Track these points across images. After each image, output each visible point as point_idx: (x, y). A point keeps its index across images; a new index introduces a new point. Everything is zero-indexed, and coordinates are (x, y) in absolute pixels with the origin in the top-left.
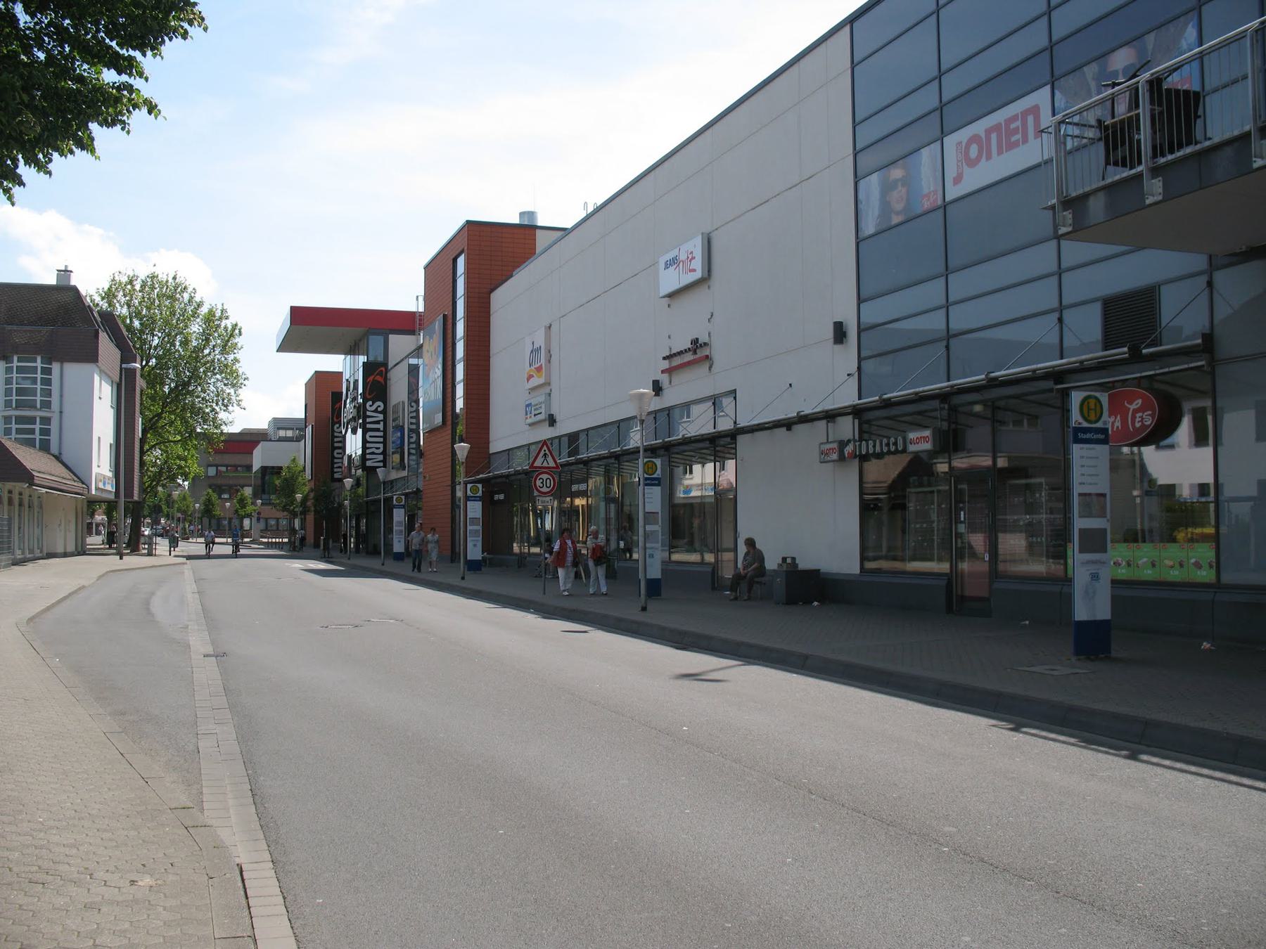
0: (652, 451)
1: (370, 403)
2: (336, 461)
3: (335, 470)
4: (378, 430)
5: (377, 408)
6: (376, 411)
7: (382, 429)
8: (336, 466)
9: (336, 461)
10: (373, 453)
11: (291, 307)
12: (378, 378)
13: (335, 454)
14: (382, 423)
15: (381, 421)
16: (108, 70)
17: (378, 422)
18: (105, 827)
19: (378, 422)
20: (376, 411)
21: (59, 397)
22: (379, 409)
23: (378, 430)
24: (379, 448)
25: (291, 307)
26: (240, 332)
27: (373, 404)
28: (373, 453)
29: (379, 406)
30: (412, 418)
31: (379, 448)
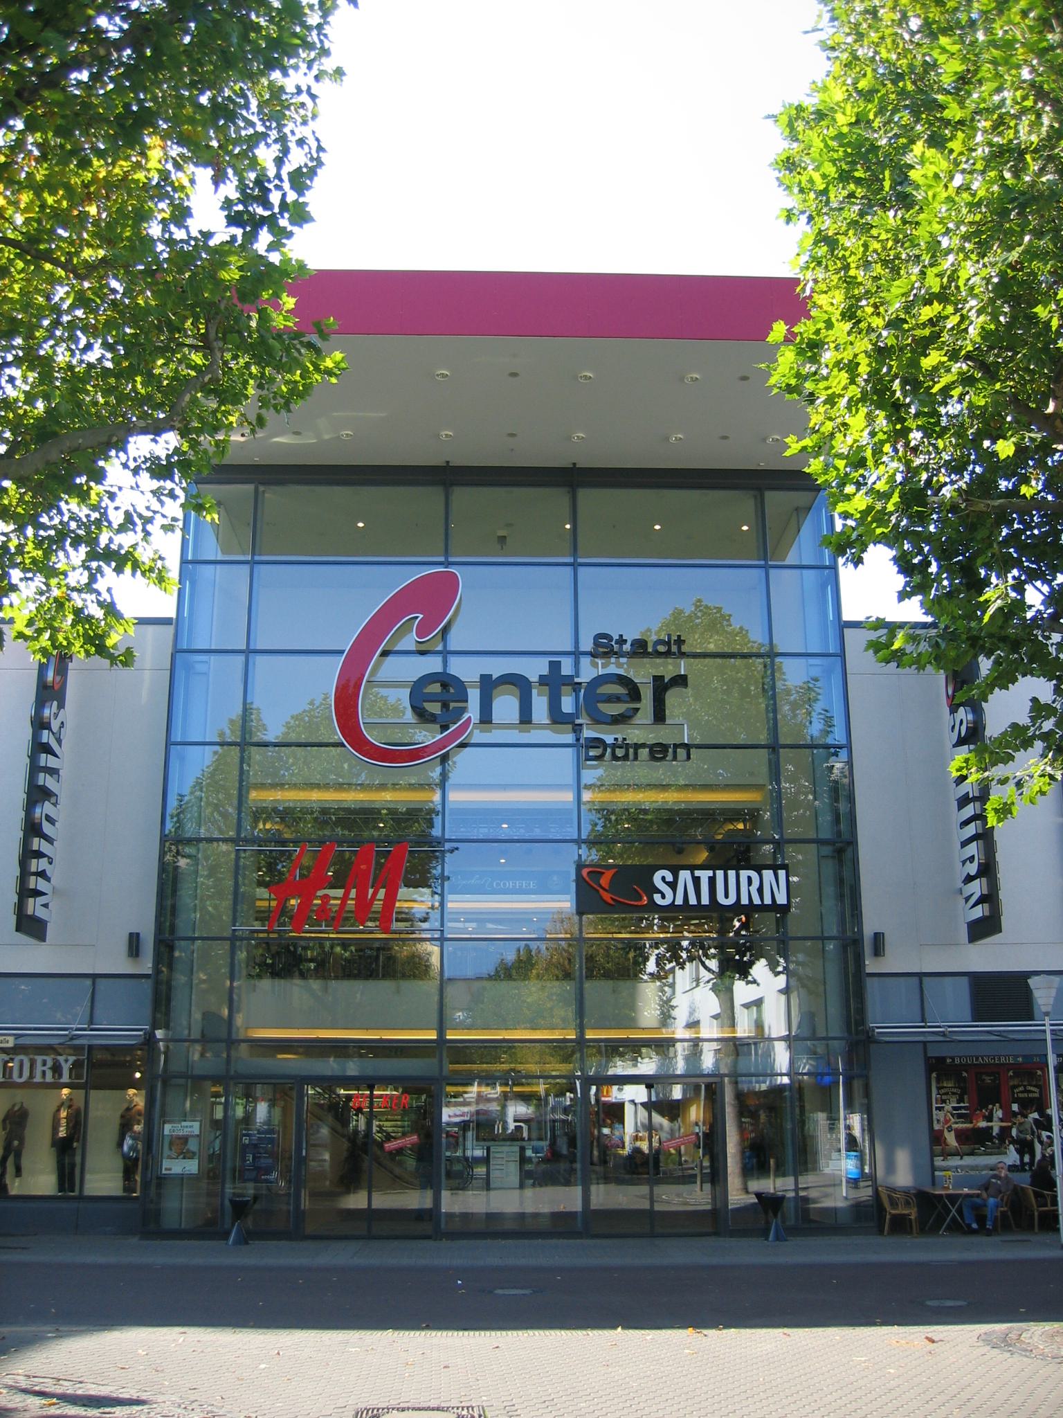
0: (779, 792)
1: (657, 897)
2: (744, 901)
3: (768, 901)
4: (712, 880)
5: (668, 883)
6: (673, 885)
7: (710, 873)
8: (757, 901)
9: (744, 901)
10: (760, 890)
11: (17, 930)
12: (604, 881)
13: (731, 900)
14: (697, 873)
15: (692, 874)
16: (898, 572)
17: (696, 881)
18: (720, 697)
19: (696, 881)
20: (673, 885)
21: (561, 460)
22: (669, 878)
23: (712, 880)
24: (750, 879)
25: (17, 930)
26: (295, 393)
27: (659, 891)
28: (760, 890)
29: (663, 878)
30: (526, 718)
31: (750, 879)
